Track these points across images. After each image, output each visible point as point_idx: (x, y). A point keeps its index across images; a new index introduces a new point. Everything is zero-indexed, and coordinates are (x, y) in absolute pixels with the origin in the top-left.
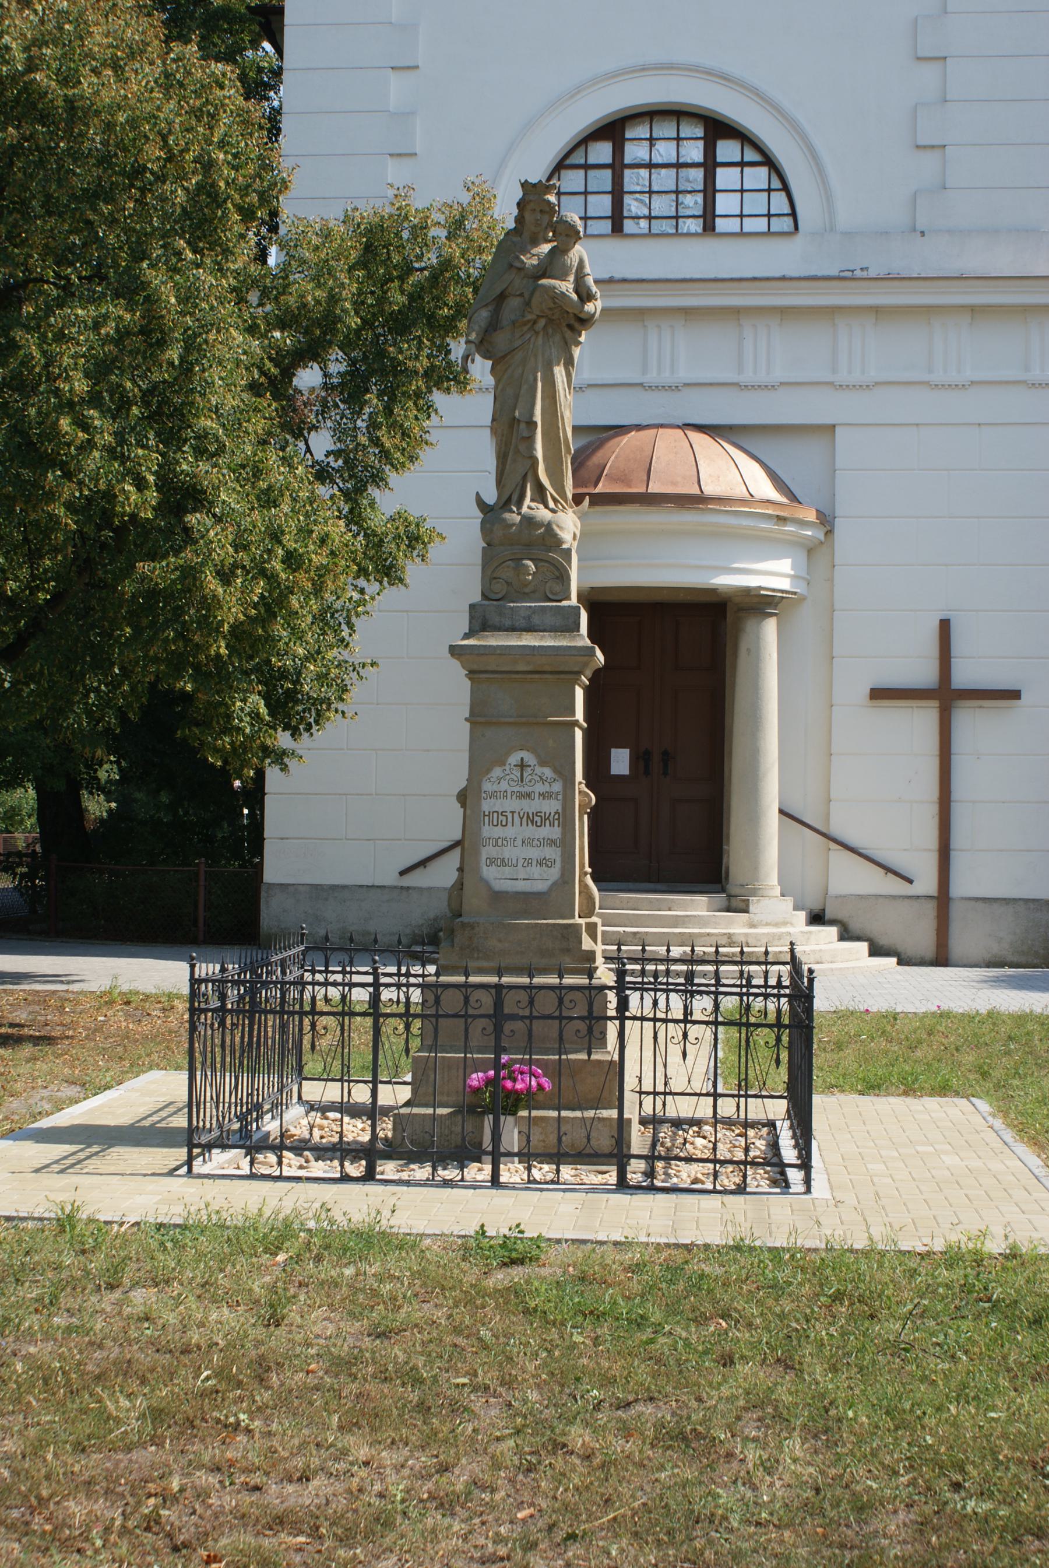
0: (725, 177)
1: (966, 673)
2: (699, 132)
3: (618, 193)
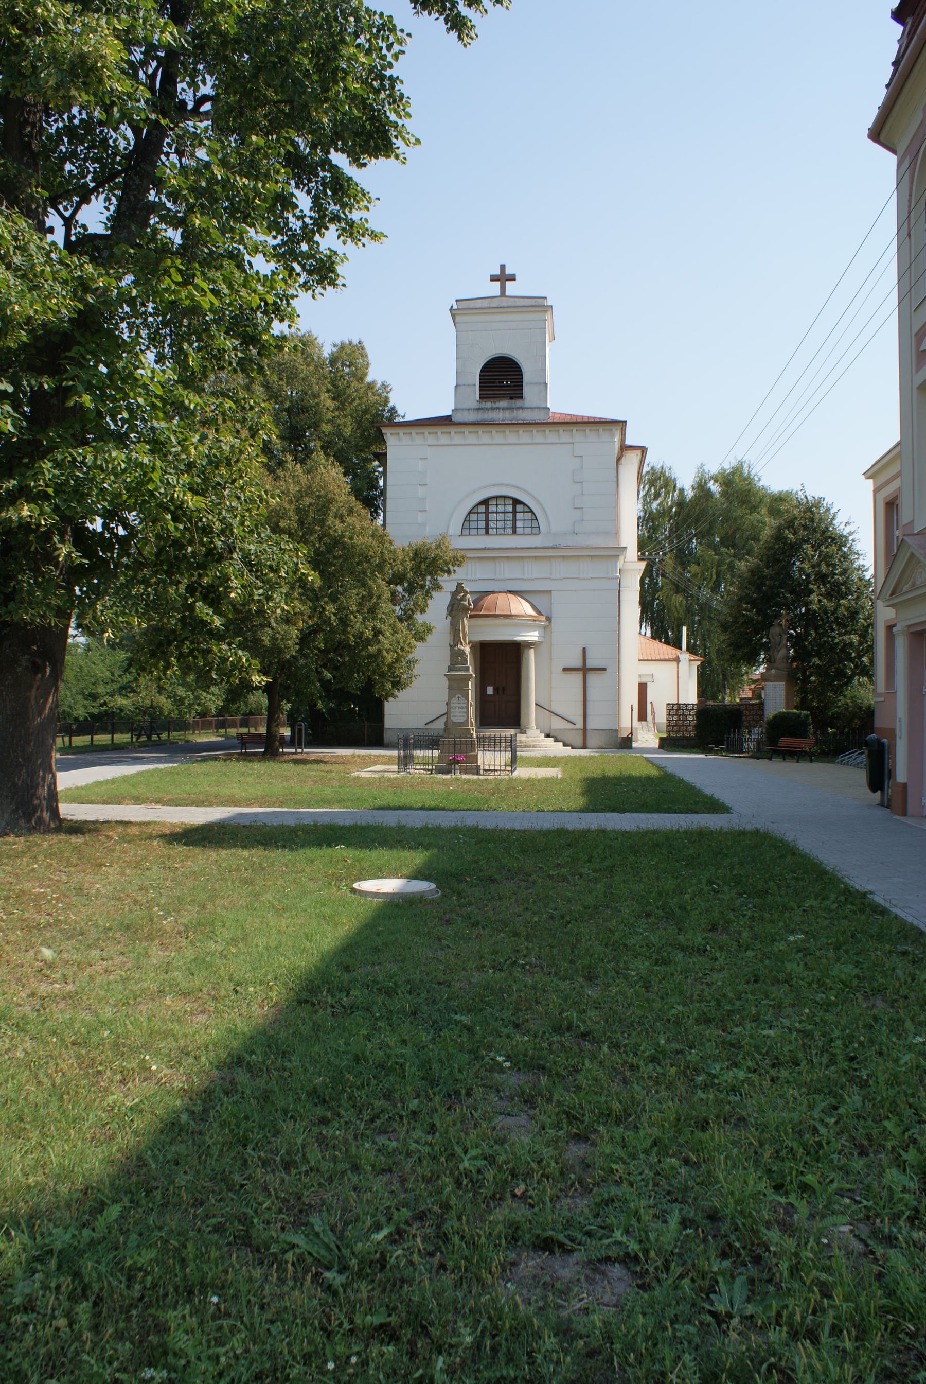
0: (519, 516)
3: (487, 521)
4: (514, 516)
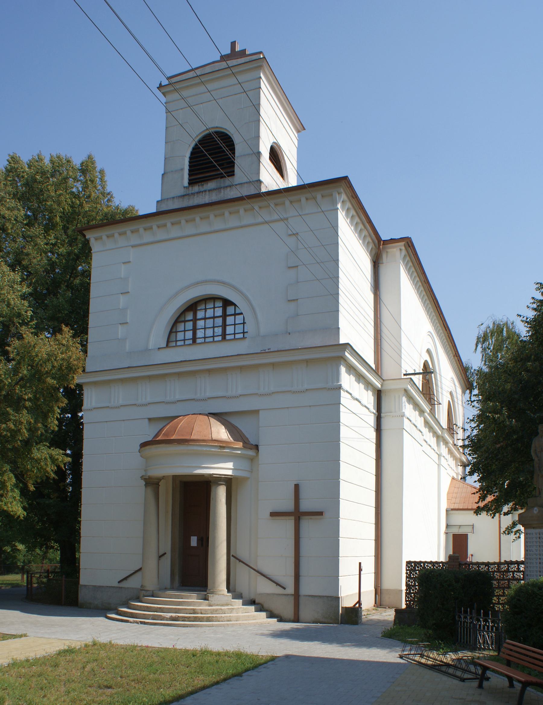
1: (289, 506)
2: (221, 304)
4: (224, 321)
